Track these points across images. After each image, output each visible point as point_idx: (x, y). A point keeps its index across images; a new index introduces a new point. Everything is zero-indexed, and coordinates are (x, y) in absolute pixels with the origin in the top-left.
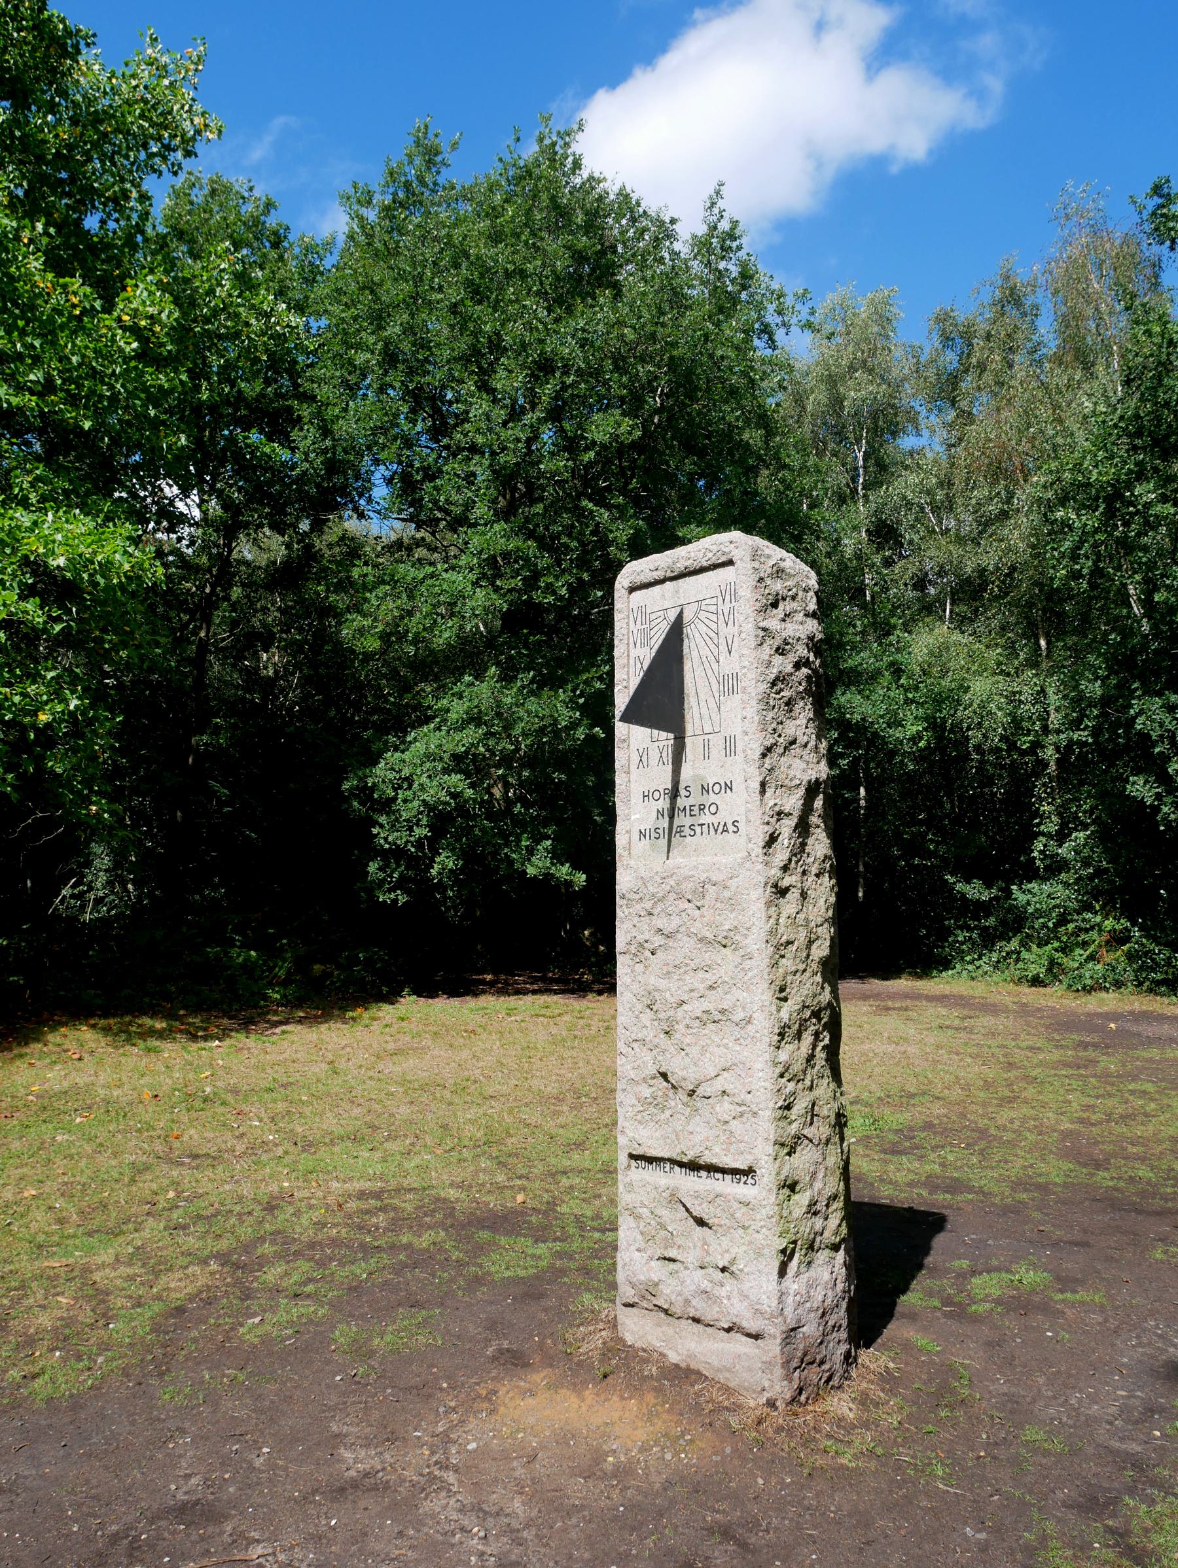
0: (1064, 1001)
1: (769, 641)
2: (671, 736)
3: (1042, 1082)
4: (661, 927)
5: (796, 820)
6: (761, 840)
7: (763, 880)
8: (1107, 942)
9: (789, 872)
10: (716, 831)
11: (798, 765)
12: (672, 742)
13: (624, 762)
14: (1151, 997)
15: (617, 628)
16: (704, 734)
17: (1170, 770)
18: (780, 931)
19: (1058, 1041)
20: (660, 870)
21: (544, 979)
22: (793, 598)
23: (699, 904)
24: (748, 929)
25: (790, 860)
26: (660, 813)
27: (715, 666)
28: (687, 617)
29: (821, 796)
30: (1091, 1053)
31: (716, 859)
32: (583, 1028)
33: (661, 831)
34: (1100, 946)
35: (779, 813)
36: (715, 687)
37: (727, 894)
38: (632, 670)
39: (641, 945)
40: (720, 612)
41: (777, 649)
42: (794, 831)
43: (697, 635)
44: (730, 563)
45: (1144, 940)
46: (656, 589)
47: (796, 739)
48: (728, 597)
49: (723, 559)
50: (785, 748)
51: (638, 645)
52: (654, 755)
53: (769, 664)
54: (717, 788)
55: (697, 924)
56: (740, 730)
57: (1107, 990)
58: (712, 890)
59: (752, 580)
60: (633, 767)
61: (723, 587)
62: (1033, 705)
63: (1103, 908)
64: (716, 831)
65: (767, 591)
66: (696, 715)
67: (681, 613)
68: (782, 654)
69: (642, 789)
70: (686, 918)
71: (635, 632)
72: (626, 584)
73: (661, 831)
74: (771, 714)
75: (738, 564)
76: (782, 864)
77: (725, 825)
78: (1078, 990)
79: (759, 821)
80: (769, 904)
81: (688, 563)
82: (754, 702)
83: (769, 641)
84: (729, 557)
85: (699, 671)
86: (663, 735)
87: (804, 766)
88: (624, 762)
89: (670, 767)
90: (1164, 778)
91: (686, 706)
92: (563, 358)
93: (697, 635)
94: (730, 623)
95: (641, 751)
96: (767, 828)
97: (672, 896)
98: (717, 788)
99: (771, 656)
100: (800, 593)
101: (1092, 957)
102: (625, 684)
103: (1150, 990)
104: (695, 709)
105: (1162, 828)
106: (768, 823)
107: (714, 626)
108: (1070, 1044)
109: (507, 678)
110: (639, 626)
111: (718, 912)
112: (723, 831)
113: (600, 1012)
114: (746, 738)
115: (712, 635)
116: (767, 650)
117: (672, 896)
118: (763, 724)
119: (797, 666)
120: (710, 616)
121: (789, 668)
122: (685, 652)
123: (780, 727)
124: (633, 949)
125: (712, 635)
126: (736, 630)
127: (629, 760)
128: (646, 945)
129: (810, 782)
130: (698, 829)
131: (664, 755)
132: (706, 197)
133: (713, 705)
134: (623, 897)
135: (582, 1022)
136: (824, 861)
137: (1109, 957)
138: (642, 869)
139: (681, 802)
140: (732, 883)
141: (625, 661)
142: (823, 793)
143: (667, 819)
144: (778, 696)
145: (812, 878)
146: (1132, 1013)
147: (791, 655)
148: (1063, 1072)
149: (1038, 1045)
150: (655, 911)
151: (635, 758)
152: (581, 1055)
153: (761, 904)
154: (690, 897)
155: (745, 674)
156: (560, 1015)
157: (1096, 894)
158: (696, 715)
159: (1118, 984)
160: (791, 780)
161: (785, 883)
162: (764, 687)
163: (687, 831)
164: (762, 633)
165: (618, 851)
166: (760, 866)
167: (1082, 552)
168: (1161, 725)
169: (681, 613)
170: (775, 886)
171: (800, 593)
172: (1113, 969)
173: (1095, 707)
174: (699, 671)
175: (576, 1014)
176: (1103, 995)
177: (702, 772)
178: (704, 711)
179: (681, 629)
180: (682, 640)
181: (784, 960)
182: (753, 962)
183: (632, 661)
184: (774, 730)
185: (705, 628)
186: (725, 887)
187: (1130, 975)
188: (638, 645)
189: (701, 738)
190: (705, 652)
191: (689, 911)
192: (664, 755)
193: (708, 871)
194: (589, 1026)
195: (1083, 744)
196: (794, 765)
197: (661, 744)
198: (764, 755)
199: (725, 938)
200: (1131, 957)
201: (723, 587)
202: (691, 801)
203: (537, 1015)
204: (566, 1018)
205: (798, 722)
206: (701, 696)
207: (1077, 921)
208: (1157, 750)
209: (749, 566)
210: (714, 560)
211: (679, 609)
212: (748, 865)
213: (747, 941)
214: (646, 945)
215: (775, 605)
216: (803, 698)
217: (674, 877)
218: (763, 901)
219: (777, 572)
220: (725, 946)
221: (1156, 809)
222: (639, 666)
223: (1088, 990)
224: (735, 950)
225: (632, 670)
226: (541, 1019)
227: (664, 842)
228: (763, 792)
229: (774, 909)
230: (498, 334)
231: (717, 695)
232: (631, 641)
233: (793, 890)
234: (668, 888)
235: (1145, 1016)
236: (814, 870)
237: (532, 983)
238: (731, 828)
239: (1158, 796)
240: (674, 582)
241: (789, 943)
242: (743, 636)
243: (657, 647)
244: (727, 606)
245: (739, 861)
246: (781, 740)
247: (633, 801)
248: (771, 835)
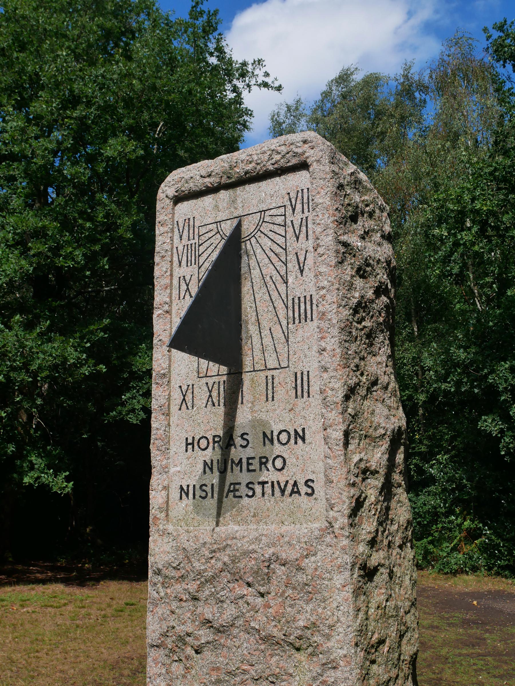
0: (438, 582)
1: (350, 260)
2: (224, 369)
3: (454, 663)
4: (209, 616)
5: (382, 480)
6: (346, 508)
7: (348, 559)
8: (465, 538)
9: (377, 546)
10: (283, 491)
11: (380, 409)
12: (225, 378)
13: (163, 401)
14: (498, 578)
15: (158, 244)
16: (267, 369)
17: (511, 413)
18: (371, 628)
19: (448, 619)
20: (208, 540)
21: (52, 569)
22: (371, 215)
23: (262, 590)
24: (330, 627)
25: (377, 531)
26: (208, 466)
27: (282, 288)
28: (248, 227)
29: (402, 448)
30: (475, 631)
31: (284, 529)
32: (84, 617)
33: (208, 489)
34: (460, 540)
35: (365, 471)
36: (282, 313)
37: (301, 578)
38: (175, 292)
39: (181, 639)
40: (289, 222)
41: (359, 270)
42: (380, 493)
43: (259, 251)
44: (304, 166)
45: (493, 537)
46: (208, 200)
47: (377, 380)
48: (299, 207)
49: (294, 161)
50: (368, 389)
51: (184, 263)
52: (202, 395)
53: (351, 287)
54: (284, 437)
55: (260, 616)
56: (316, 365)
57: (467, 573)
58: (280, 571)
59: (331, 186)
60: (174, 409)
61: (293, 195)
62: (413, 366)
63: (461, 513)
64: (283, 491)
65: (347, 201)
66: (257, 346)
67: (239, 226)
68: (363, 277)
69: (184, 435)
70: (244, 608)
71: (181, 248)
72: (171, 192)
73: (208, 489)
74: (354, 347)
75: (314, 167)
76: (369, 537)
77: (295, 484)
78: (447, 573)
79: (343, 482)
80: (358, 592)
81: (250, 167)
82: (335, 331)
83: (350, 260)
84: (303, 158)
85: (261, 294)
86: (214, 368)
87: (386, 412)
88: (163, 401)
89: (221, 410)
90: (506, 418)
91: (244, 335)
92: (87, 97)
93: (259, 251)
94: (303, 236)
95: (184, 388)
96: (353, 491)
97: (226, 576)
98: (284, 437)
99: (352, 276)
100: (377, 211)
101: (455, 549)
102: (166, 307)
103: (498, 574)
104: (256, 339)
105: (503, 453)
106: (354, 485)
107: (280, 240)
108: (457, 622)
109: (29, 326)
110: (185, 241)
111: (288, 602)
112: (292, 492)
113: (98, 600)
114: (325, 375)
115: (278, 250)
116: (349, 271)
117: (226, 576)
118: (346, 357)
119: (379, 291)
120: (276, 228)
121: (370, 294)
122: (243, 271)
123: (362, 363)
124: (169, 642)
125: (278, 250)
126: (310, 244)
127: (169, 399)
128: (188, 639)
129: (393, 430)
130: (258, 489)
131: (215, 394)
132: (189, 11)
133: (278, 334)
134: (158, 572)
135: (83, 611)
136: (406, 528)
137: (466, 549)
138: (184, 537)
139: (236, 453)
140: (309, 563)
141: (168, 281)
142: (405, 445)
143: (217, 474)
144: (360, 326)
145: (396, 551)
146: (490, 592)
147: (372, 279)
148: (464, 651)
149: (435, 624)
150: (199, 595)
151: (177, 396)
152: (83, 647)
153: (348, 593)
154: (250, 580)
155: (323, 297)
156: (65, 605)
157: (456, 502)
158: (257, 346)
159: (475, 569)
160: (376, 429)
161: (373, 562)
162: (346, 313)
163: (243, 490)
164: (342, 250)
165: (153, 512)
166: (345, 542)
167: (452, 259)
168: (506, 381)
169: (239, 226)
170: (364, 567)
171: (377, 211)
172: (471, 558)
173: (459, 368)
174: (261, 294)
175: (78, 604)
176: (465, 577)
177: (263, 416)
178: (268, 340)
179: (240, 243)
180: (240, 257)
181: (375, 667)
182: (339, 673)
183: (175, 282)
184: (357, 366)
185: (270, 243)
186: (299, 569)
187: (482, 562)
188: (184, 263)
189: (263, 374)
190: (269, 270)
191: (250, 599)
192: (215, 394)
193: (274, 545)
194: (89, 614)
195: (446, 393)
196: (377, 411)
197: (210, 381)
198: (347, 398)
199: (300, 638)
200: (484, 549)
201: (293, 195)
202: (249, 452)
203: (46, 606)
204: (70, 608)
205: (379, 359)
206: (264, 323)
207: (445, 523)
208: (503, 398)
209: (327, 169)
210: (283, 163)
211: (235, 222)
212: (328, 539)
213: (330, 644)
214: (188, 639)
215: (354, 219)
216: (382, 331)
217: (228, 551)
218: (350, 588)
219: (355, 182)
220: (298, 649)
221: (498, 440)
222: (184, 287)
223: (455, 573)
224: (312, 655)
225: (175, 292)
226: (50, 609)
227: (211, 503)
228: (346, 444)
229: (363, 598)
230: (37, 74)
231: (284, 323)
232: (175, 259)
233: (382, 570)
234: (220, 565)
235: (499, 595)
236: (398, 541)
237: (41, 573)
238: (304, 489)
239: (502, 431)
240: (231, 192)
241: (381, 642)
242: (320, 250)
243: (207, 265)
244: (297, 218)
245: (317, 533)
246: (364, 379)
247: (173, 449)
248: (357, 500)
